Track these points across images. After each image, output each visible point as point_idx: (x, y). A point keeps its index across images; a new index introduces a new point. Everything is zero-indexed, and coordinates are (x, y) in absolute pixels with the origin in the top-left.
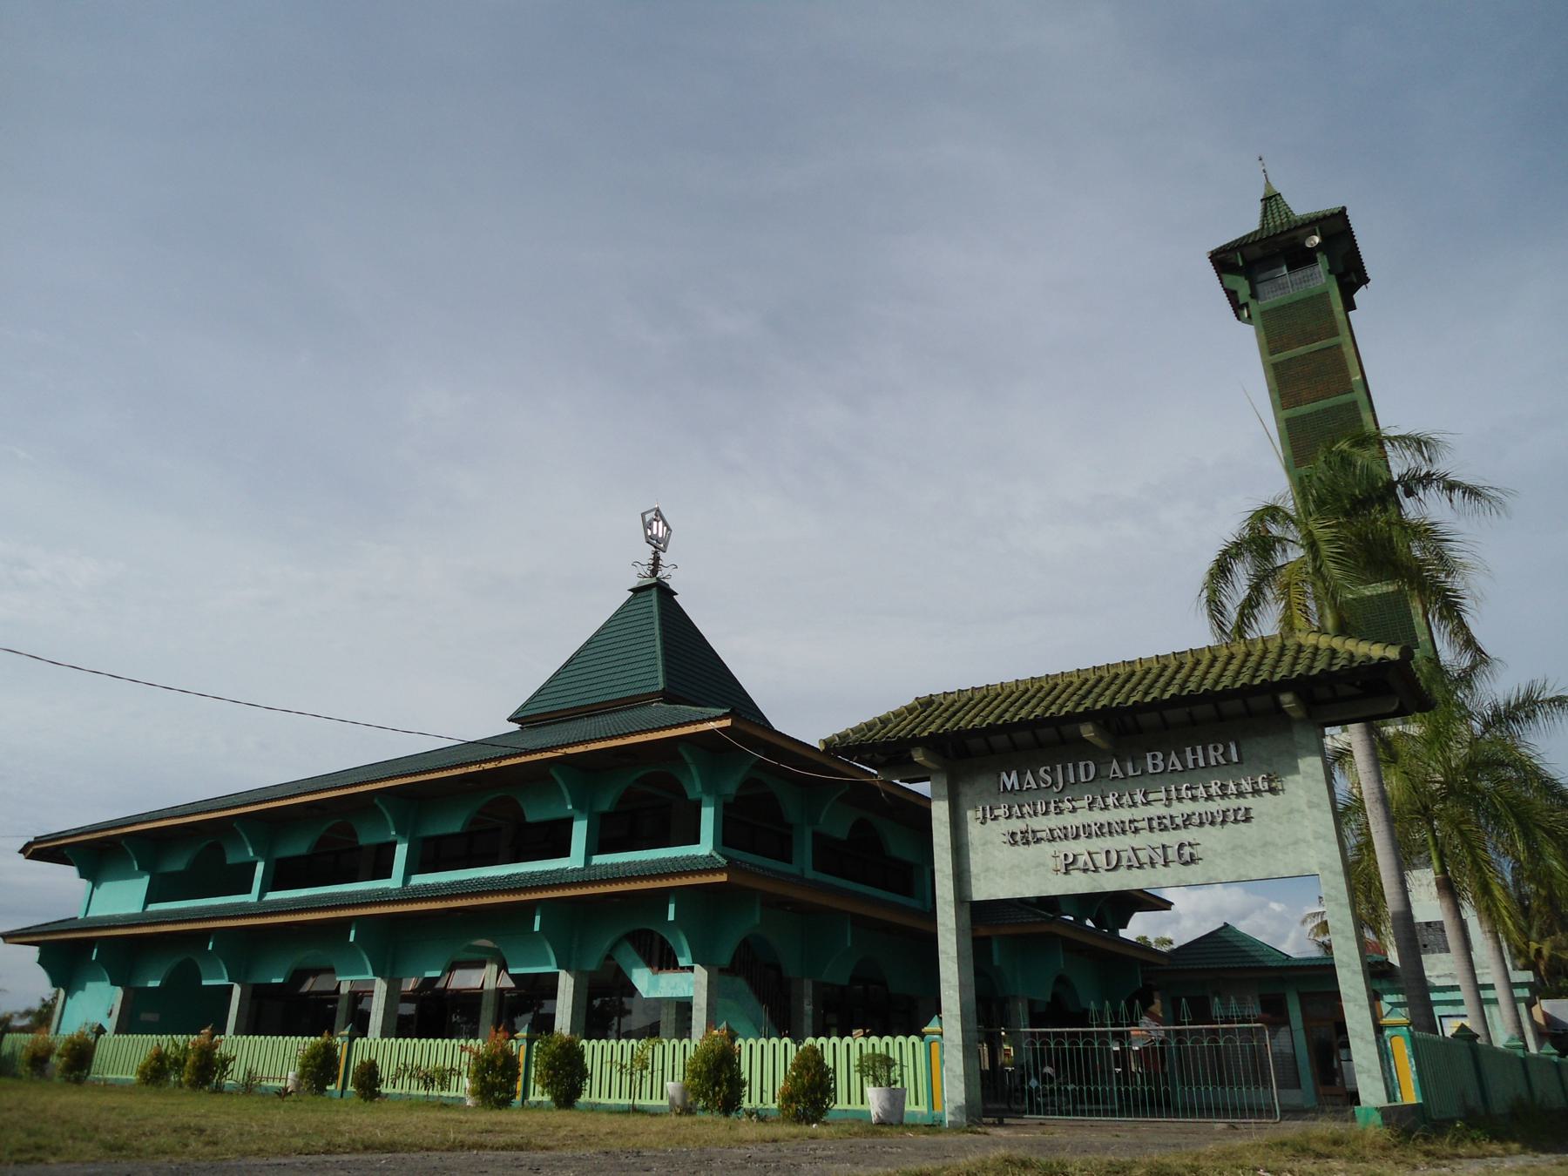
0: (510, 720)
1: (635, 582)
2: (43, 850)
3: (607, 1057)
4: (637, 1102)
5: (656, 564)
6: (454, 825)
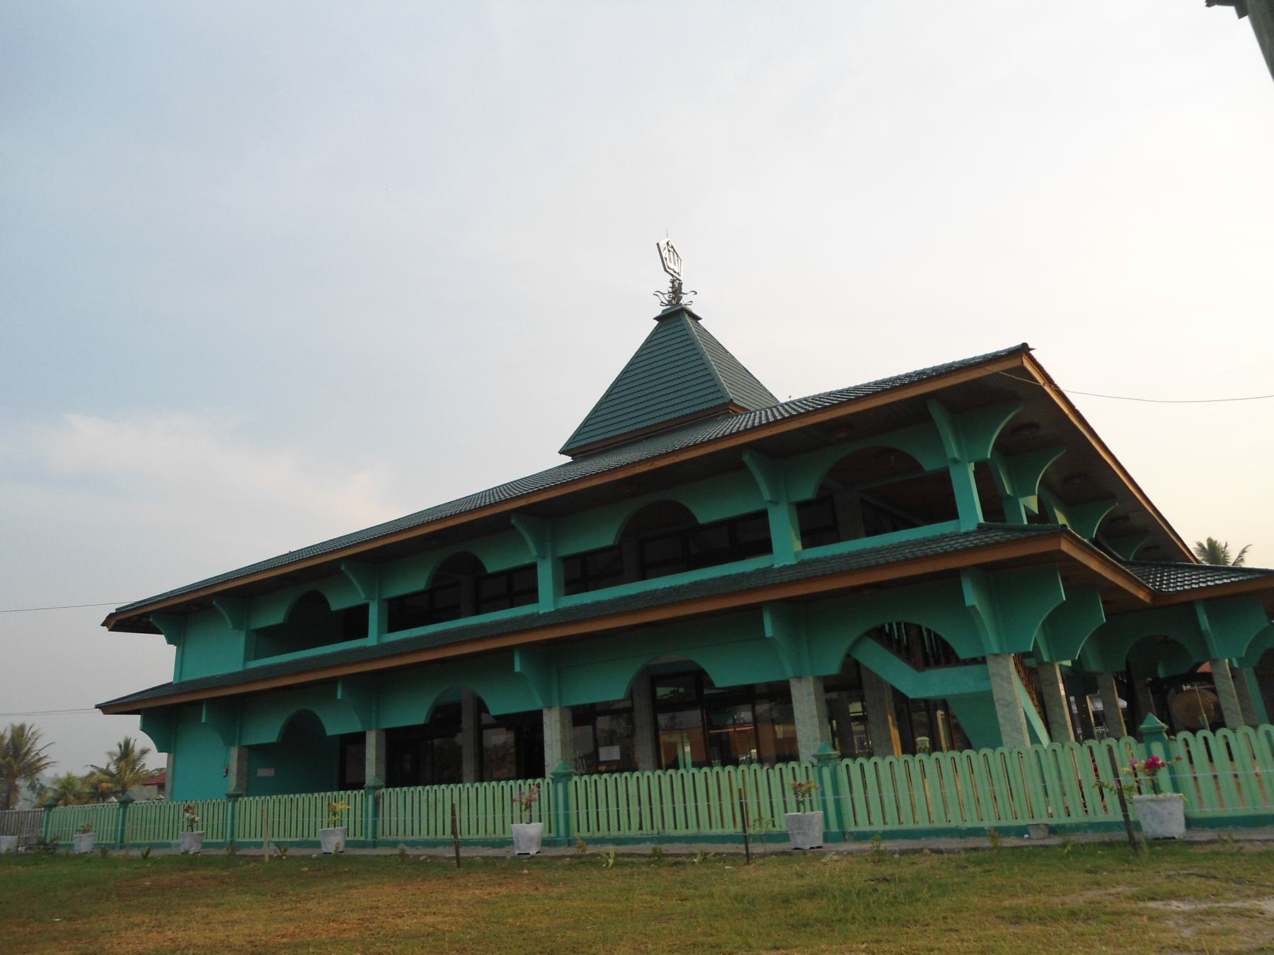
0: (561, 452)
1: (659, 311)
3: (507, 795)
4: (170, 840)
5: (677, 291)
6: (605, 537)
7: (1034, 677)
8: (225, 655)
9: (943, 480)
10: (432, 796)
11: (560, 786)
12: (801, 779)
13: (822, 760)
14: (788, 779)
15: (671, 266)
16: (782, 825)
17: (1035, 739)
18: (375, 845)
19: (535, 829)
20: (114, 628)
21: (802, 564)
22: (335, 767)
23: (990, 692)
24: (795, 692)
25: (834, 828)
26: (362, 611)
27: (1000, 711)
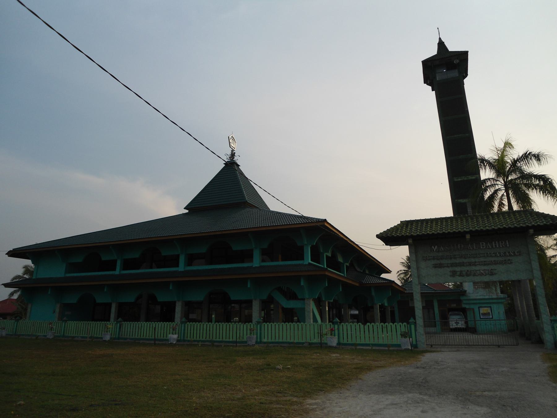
2: (15, 253)
5: (233, 155)
7: (319, 303)
8: (56, 271)
9: (302, 249)
10: (140, 325)
11: (183, 325)
12: (252, 327)
13: (258, 323)
14: (249, 327)
15: (232, 145)
16: (245, 339)
17: (315, 320)
18: (119, 338)
19: (175, 336)
20: (10, 256)
21: (261, 267)
22: (100, 314)
23: (304, 308)
24: (254, 303)
25: (259, 340)
26: (115, 262)
27: (306, 313)
